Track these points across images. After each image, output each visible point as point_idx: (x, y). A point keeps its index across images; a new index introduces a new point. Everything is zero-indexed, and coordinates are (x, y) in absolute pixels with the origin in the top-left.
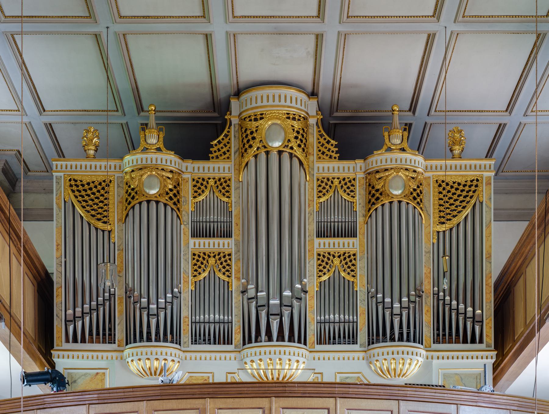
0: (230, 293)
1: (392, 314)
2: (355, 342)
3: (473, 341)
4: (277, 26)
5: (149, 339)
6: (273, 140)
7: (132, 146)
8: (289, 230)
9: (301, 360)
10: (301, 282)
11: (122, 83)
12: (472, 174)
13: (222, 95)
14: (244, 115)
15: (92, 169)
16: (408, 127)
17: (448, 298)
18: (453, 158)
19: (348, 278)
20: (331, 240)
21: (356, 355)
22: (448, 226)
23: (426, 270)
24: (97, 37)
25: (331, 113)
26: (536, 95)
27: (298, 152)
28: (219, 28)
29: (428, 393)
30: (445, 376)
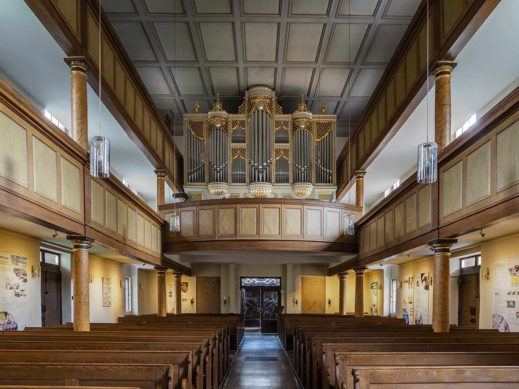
0: (245, 164)
1: (301, 172)
2: (288, 183)
3: (329, 182)
4: (261, 65)
5: (217, 181)
6: (260, 107)
7: (211, 108)
8: (22, 120)
9: (270, 189)
10: (270, 160)
11: (208, 85)
12: (329, 120)
13: (242, 89)
14: (250, 97)
15: (198, 117)
16: (307, 102)
17: (325, 169)
18: (322, 114)
19: (286, 158)
20: (280, 144)
21: (289, 187)
22: (320, 139)
23: (313, 156)
24: (199, 68)
25: (280, 96)
26: (350, 91)
27: (269, 111)
28: (241, 65)
29: (313, 202)
30: (320, 195)
